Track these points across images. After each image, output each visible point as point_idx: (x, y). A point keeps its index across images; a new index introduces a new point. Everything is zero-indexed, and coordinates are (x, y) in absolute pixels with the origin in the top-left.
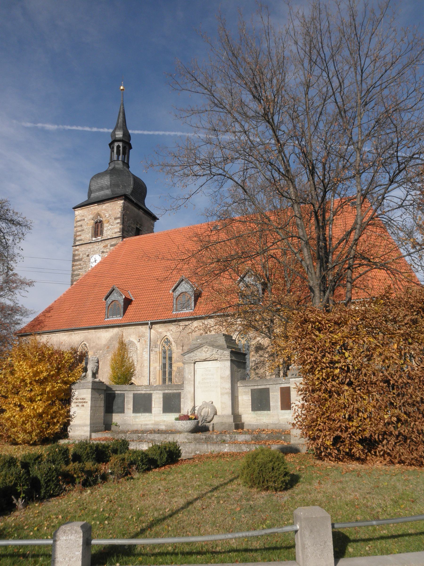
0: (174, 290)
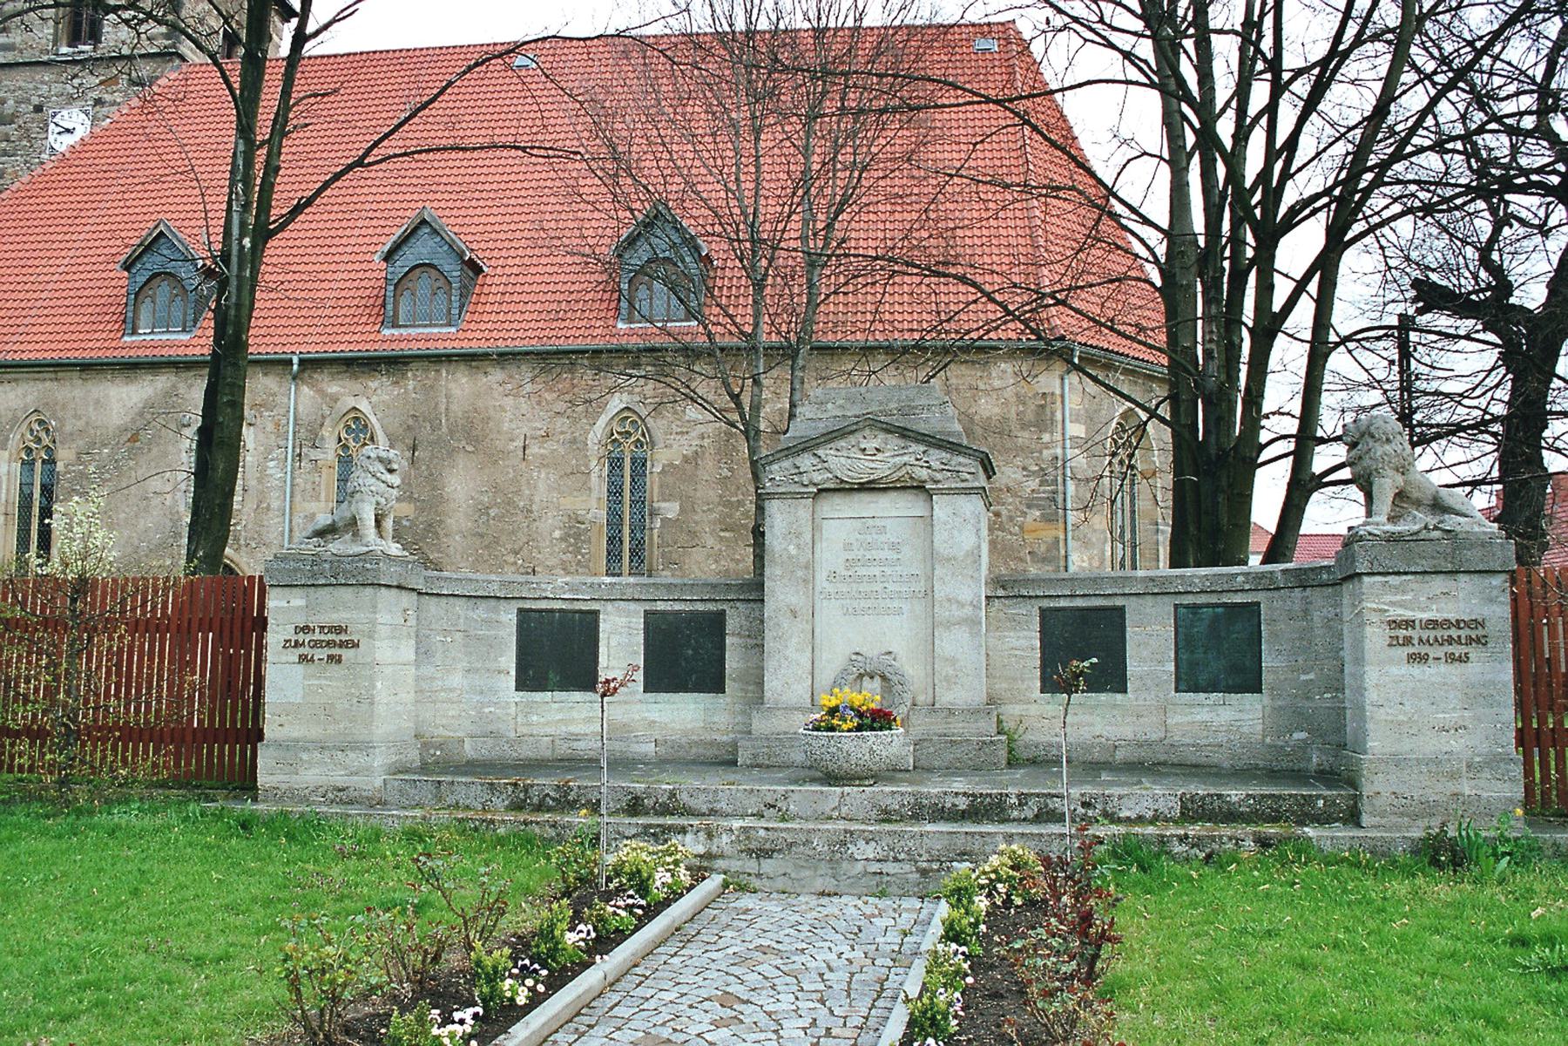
0: (388, 257)
